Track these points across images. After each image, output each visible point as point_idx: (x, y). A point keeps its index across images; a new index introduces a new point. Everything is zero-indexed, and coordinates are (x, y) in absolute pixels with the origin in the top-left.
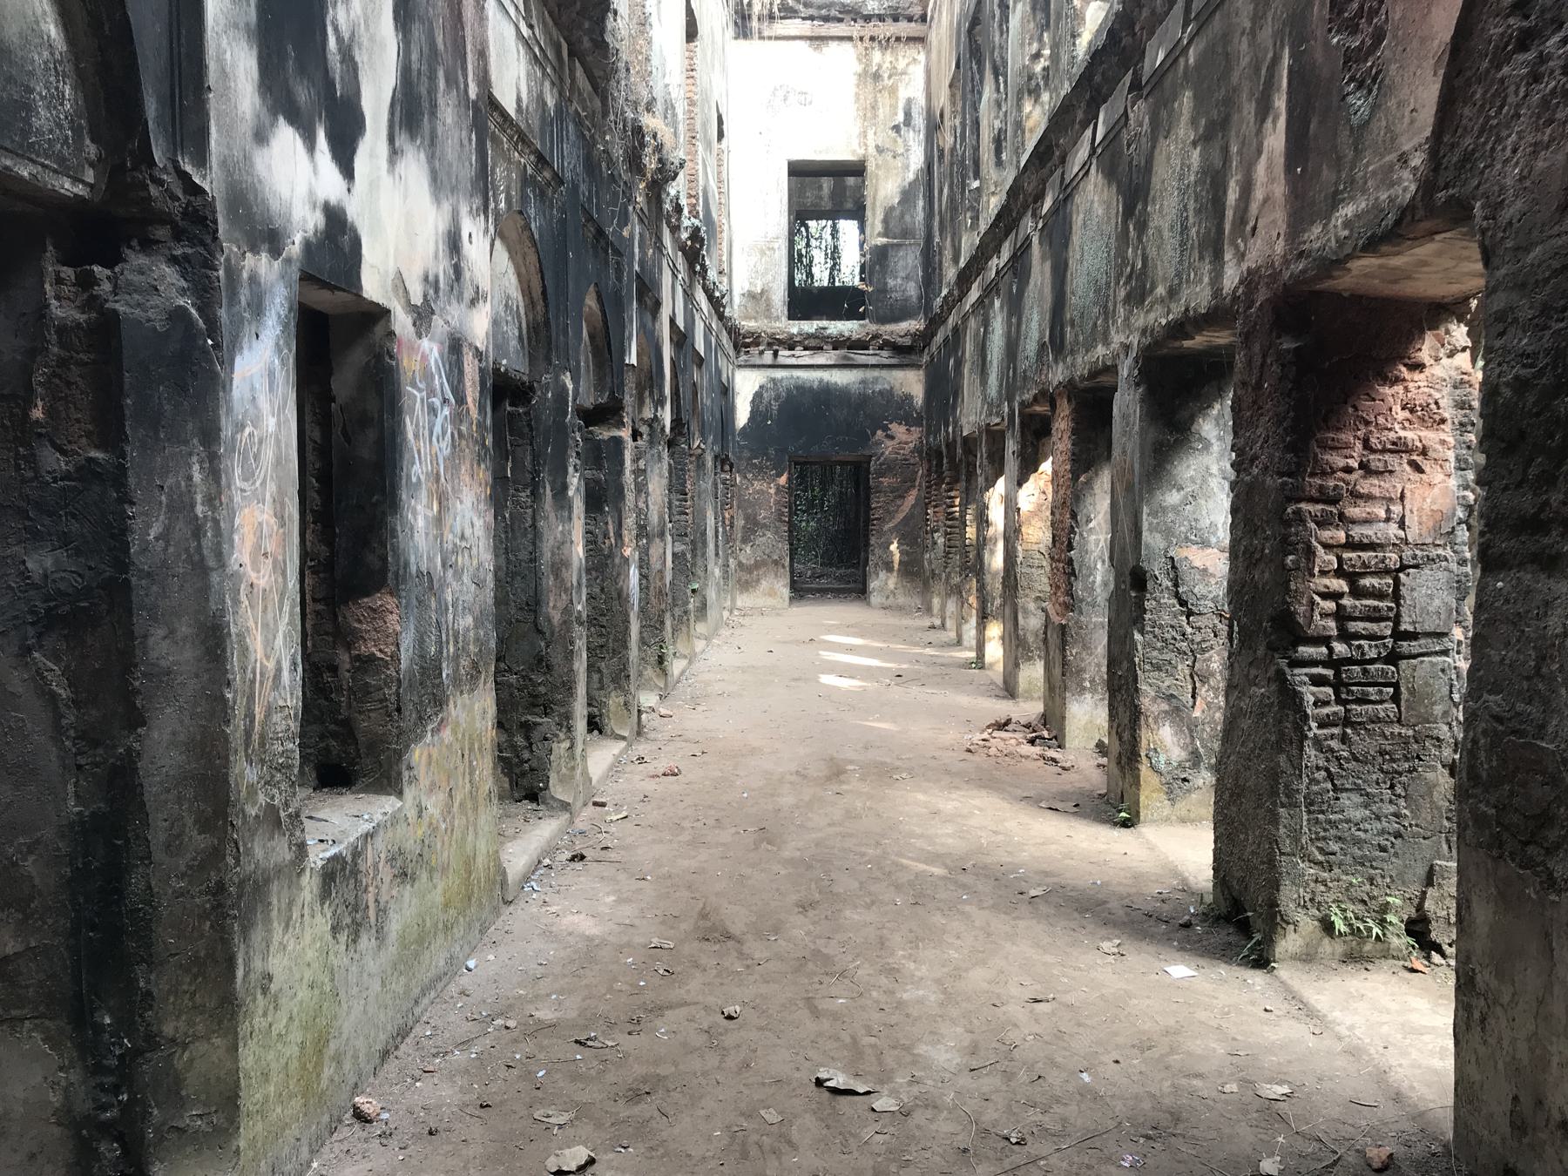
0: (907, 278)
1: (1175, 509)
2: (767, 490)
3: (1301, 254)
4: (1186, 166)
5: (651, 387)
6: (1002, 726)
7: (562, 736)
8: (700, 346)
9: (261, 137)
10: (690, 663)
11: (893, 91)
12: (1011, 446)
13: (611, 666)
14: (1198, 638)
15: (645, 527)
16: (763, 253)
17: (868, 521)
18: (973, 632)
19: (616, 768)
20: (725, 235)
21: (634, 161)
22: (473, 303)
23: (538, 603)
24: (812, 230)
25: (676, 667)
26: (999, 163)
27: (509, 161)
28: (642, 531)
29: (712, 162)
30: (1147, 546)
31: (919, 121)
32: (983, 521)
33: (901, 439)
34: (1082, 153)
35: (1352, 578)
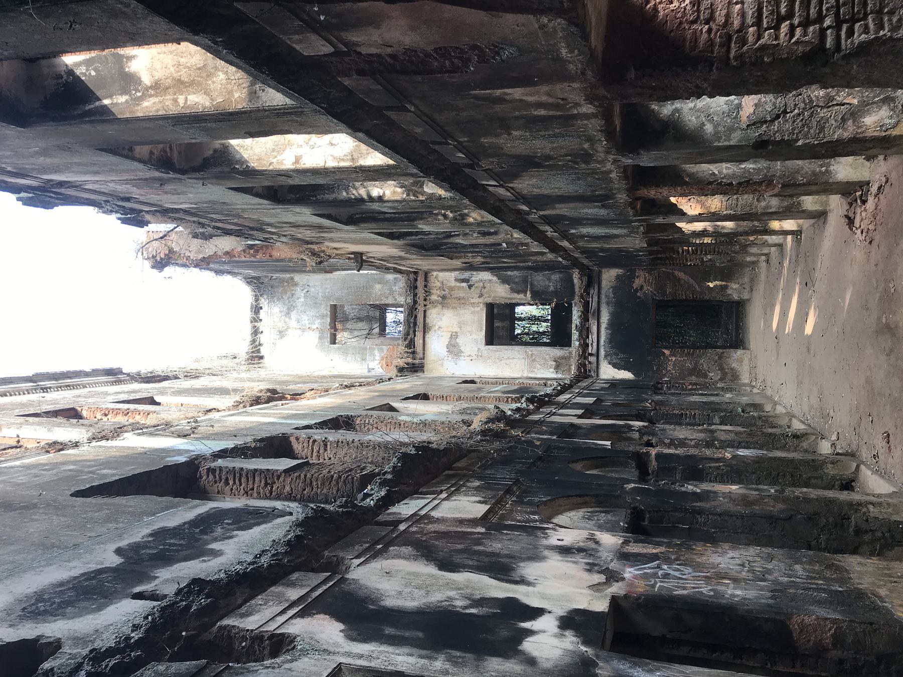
0: (549, 279)
1: (716, 126)
2: (673, 362)
3: (583, 73)
4: (520, 138)
5: (620, 432)
6: (850, 221)
7: (864, 510)
8: (590, 400)
9: (531, 661)
10: (795, 417)
11: (451, 289)
12: (660, 220)
13: (810, 470)
14: (802, 105)
15: (707, 442)
16: (534, 360)
17: (694, 300)
18: (774, 237)
19: (883, 474)
20: (525, 381)
21: (498, 435)
22: (597, 542)
23: (771, 517)
24: (519, 332)
25: (797, 426)
26: (496, 233)
27: (512, 510)
28: (709, 445)
29: (488, 388)
30: (740, 141)
31: (466, 275)
32: (703, 233)
33: (642, 281)
34: (501, 191)
35: (780, 19)
